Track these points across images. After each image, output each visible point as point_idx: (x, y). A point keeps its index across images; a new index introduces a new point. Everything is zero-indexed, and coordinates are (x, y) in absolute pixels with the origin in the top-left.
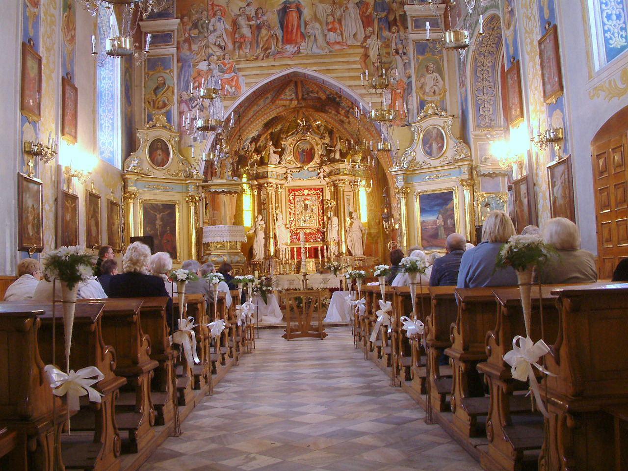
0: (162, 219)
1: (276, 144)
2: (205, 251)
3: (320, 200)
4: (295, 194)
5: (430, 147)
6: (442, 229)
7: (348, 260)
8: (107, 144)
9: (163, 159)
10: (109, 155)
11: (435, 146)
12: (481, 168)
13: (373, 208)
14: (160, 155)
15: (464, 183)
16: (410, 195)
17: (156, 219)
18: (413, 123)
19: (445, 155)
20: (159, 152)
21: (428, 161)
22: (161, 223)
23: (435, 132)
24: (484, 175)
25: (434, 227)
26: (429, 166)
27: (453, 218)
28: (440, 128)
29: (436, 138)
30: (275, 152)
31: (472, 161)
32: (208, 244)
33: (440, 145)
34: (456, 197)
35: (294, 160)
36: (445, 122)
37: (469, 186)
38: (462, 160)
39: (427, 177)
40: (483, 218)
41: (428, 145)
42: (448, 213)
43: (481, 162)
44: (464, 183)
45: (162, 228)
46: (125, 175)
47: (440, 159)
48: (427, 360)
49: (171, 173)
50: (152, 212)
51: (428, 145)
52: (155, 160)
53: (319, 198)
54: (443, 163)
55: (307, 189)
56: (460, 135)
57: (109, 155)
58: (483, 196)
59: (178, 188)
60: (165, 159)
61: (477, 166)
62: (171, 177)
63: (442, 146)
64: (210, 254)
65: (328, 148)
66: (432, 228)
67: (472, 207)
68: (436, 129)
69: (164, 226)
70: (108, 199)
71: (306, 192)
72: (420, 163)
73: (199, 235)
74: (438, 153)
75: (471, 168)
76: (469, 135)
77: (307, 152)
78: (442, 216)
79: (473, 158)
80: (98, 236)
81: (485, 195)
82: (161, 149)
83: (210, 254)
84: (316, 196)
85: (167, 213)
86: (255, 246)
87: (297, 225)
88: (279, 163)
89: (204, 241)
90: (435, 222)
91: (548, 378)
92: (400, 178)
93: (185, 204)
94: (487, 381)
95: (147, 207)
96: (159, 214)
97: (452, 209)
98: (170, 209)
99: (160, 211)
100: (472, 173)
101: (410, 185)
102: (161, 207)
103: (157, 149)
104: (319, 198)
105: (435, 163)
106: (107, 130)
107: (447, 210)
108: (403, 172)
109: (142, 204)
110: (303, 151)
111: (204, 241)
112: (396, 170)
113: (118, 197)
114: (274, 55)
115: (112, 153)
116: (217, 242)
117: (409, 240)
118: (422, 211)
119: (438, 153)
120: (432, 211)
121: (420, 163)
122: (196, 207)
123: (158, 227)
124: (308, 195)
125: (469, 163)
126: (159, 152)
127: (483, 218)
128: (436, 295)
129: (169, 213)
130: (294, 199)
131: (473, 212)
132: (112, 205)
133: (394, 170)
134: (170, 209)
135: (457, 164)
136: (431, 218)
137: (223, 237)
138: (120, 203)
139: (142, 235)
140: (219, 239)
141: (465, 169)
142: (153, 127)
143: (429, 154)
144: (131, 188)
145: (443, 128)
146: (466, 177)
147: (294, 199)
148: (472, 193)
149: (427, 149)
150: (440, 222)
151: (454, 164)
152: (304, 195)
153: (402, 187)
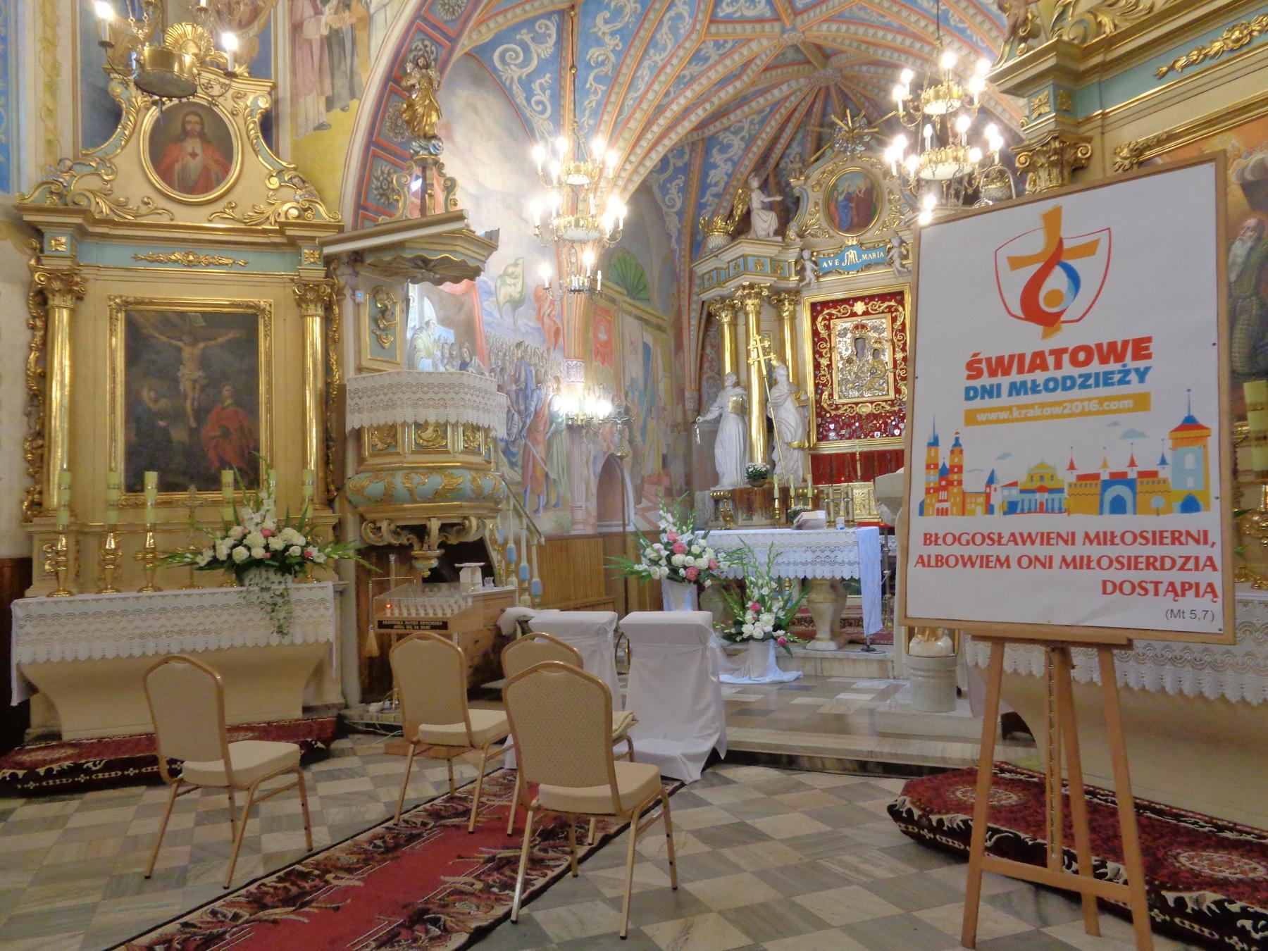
4: (830, 315)
9: (206, 171)
14: (194, 155)
17: (179, 362)
20: (193, 145)
35: (825, 225)
39: (1183, 61)
45: (203, 390)
48: (978, 638)
50: (163, 339)
52: (177, 167)
53: (894, 320)
55: (862, 299)
60: (215, 168)
69: (212, 381)
71: (859, 307)
82: (202, 136)
86: (719, 452)
87: (836, 397)
91: (313, 703)
94: (482, 852)
103: (185, 134)
110: (849, 198)
123: (185, 385)
124: (866, 313)
126: (193, 145)
130: (828, 327)
147: (828, 327)
152: (854, 314)
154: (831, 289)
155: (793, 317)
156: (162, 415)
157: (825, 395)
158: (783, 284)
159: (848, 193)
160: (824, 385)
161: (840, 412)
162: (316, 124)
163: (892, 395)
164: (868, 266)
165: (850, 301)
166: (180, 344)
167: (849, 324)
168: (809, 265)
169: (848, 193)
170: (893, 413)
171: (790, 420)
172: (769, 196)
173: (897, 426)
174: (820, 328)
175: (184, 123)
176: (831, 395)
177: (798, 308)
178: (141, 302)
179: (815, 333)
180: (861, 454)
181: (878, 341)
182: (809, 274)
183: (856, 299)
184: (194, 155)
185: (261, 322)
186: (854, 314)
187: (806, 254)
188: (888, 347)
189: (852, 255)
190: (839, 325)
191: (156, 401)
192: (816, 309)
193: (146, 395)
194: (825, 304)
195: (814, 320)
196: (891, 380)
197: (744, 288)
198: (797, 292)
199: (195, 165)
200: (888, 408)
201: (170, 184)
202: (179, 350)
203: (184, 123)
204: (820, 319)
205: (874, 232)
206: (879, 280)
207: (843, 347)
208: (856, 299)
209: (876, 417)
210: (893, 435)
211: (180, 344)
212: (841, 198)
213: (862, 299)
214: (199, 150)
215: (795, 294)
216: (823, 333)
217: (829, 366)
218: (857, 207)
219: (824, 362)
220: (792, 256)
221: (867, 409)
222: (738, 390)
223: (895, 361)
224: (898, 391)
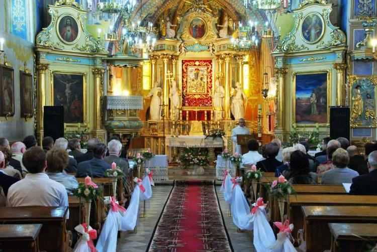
0: (71, 88)
1: (173, 20)
2: (108, 116)
3: (209, 70)
5: (309, 33)
6: (315, 106)
7: (231, 123)
8: (19, 19)
9: (72, 35)
10: (22, 29)
11: (313, 32)
12: (355, 55)
13: (254, 79)
14: (69, 31)
15: (338, 67)
16: (287, 76)
17: (65, 88)
18: (294, 10)
19: (322, 40)
20: (69, 28)
21: (306, 45)
22: (69, 92)
23: (314, 19)
24: (358, 60)
25: (308, 104)
26: (306, 50)
27: (325, 97)
28: (320, 16)
29: (315, 25)
30: (171, 28)
31: (346, 47)
32: (111, 111)
33: (318, 31)
34: (329, 78)
36: (325, 10)
37: (342, 69)
38: (337, 46)
39: (304, 60)
40: (353, 99)
41: (307, 31)
42: (322, 92)
43: (356, 48)
44: (338, 67)
46: (37, 48)
47: (317, 44)
49: (79, 47)
50: (62, 82)
51: (307, 31)
52: (65, 34)
53: (208, 68)
54: (319, 48)
55: (198, 61)
56: (338, 21)
57: (22, 29)
58: (354, 79)
59: (86, 61)
60: (74, 35)
61: (351, 53)
62: (79, 51)
63: (320, 32)
64: (112, 120)
65: (218, 25)
66: (306, 105)
67: (343, 88)
68: (315, 16)
70: (20, 71)
71: (197, 63)
72: (299, 47)
73: (103, 105)
74: (315, 39)
75: (346, 53)
76: (346, 22)
77: (199, 28)
78: (316, 95)
79: (348, 44)
80: (12, 106)
81: (357, 78)
82: (71, 25)
83: (112, 120)
84: (206, 67)
85: (75, 82)
88: (175, 37)
89: (109, 107)
90: (309, 99)
92: (280, 60)
93: (91, 75)
95: (57, 77)
96: (68, 83)
97: (325, 89)
98: (78, 79)
99: (69, 81)
100: (346, 57)
101: (288, 66)
102: (70, 78)
103: (67, 25)
104: (208, 68)
105: (313, 47)
106: (19, 6)
107: (320, 90)
108: (283, 55)
109: (52, 75)
110: (196, 27)
111: (109, 107)
112: (277, 52)
113: (30, 68)
114: (87, 19)
115: (25, 27)
116: (119, 110)
117: (285, 106)
118: (298, 89)
119: (315, 39)
120: (306, 90)
121: (299, 47)
122: (101, 79)
123: (67, 95)
124: (199, 65)
125: (343, 48)
126: (69, 28)
127: (353, 99)
128: (309, 216)
129: (77, 83)
130: (186, 69)
131: (344, 92)
132: (23, 75)
133: (275, 52)
134: (78, 79)
135: (332, 50)
136: (305, 96)
137: (124, 105)
138: (32, 74)
139: (53, 105)
140: (120, 107)
141: (339, 55)
142: (63, 4)
143: (308, 38)
144: (42, 61)
145: (322, 16)
146: (340, 61)
148: (345, 75)
149: (306, 34)
150: (314, 100)
151: (329, 49)
152: (195, 65)
153: (281, 68)
154: (189, 55)
155: (176, 64)
156: (61, 102)
157: (185, 91)
158: (175, 54)
159: (196, 26)
160: (185, 87)
161: (189, 97)
162: (96, 22)
163: (206, 93)
164: (202, 51)
165: (194, 61)
166: (66, 83)
167: (193, 68)
168: (183, 48)
169: (196, 26)
170: (206, 99)
171: (176, 101)
172: (173, 24)
173: (207, 103)
174: (184, 69)
175: (67, 22)
176: (186, 91)
177: (178, 61)
178: (57, 72)
179: (183, 70)
180: (198, 112)
181: (202, 75)
182: (183, 51)
183: (196, 61)
184: (69, 31)
185: (84, 78)
186: (195, 65)
187: (182, 45)
188: (205, 77)
189: (197, 47)
190: (190, 68)
191: (60, 99)
192: (183, 62)
193: (58, 97)
194: (186, 61)
195: (183, 65)
196: (206, 87)
197: (164, 55)
198: (178, 56)
199: (69, 34)
200: (205, 97)
201: (63, 38)
202: (65, 85)
203: (67, 22)
204: (184, 65)
205: (203, 40)
206: (205, 55)
207: (191, 75)
208: (196, 61)
209: (201, 99)
210: (206, 106)
211: (66, 83)
212: (194, 26)
213: (198, 61)
214: (70, 30)
215: (177, 57)
216: (185, 70)
217: (186, 82)
218: (199, 30)
219: (185, 80)
220: (178, 44)
221: (197, 97)
222: (159, 88)
223: (207, 82)
224: (208, 91)
